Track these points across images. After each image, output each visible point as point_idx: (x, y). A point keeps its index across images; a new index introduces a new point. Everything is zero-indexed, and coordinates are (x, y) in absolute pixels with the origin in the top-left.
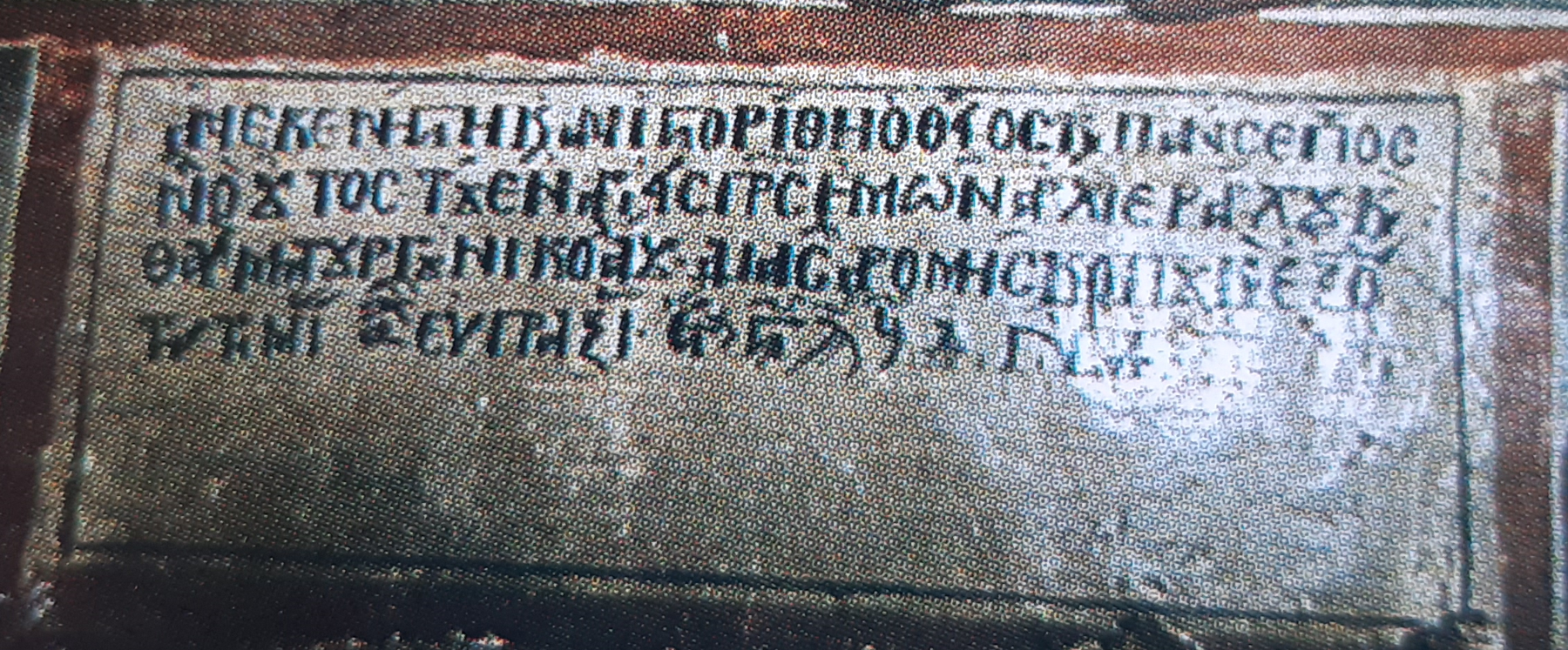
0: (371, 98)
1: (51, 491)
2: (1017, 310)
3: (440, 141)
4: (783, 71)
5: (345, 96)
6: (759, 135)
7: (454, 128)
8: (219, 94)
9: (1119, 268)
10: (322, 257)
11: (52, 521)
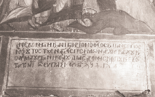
0: (38, 42)
1: (5, 81)
2: (104, 62)
3: (45, 46)
4: (80, 39)
5: (35, 42)
6: (78, 46)
7: (47, 45)
8: (22, 41)
9: (114, 58)
10: (34, 57)
11: (5, 85)
